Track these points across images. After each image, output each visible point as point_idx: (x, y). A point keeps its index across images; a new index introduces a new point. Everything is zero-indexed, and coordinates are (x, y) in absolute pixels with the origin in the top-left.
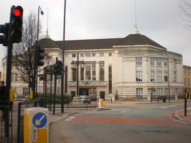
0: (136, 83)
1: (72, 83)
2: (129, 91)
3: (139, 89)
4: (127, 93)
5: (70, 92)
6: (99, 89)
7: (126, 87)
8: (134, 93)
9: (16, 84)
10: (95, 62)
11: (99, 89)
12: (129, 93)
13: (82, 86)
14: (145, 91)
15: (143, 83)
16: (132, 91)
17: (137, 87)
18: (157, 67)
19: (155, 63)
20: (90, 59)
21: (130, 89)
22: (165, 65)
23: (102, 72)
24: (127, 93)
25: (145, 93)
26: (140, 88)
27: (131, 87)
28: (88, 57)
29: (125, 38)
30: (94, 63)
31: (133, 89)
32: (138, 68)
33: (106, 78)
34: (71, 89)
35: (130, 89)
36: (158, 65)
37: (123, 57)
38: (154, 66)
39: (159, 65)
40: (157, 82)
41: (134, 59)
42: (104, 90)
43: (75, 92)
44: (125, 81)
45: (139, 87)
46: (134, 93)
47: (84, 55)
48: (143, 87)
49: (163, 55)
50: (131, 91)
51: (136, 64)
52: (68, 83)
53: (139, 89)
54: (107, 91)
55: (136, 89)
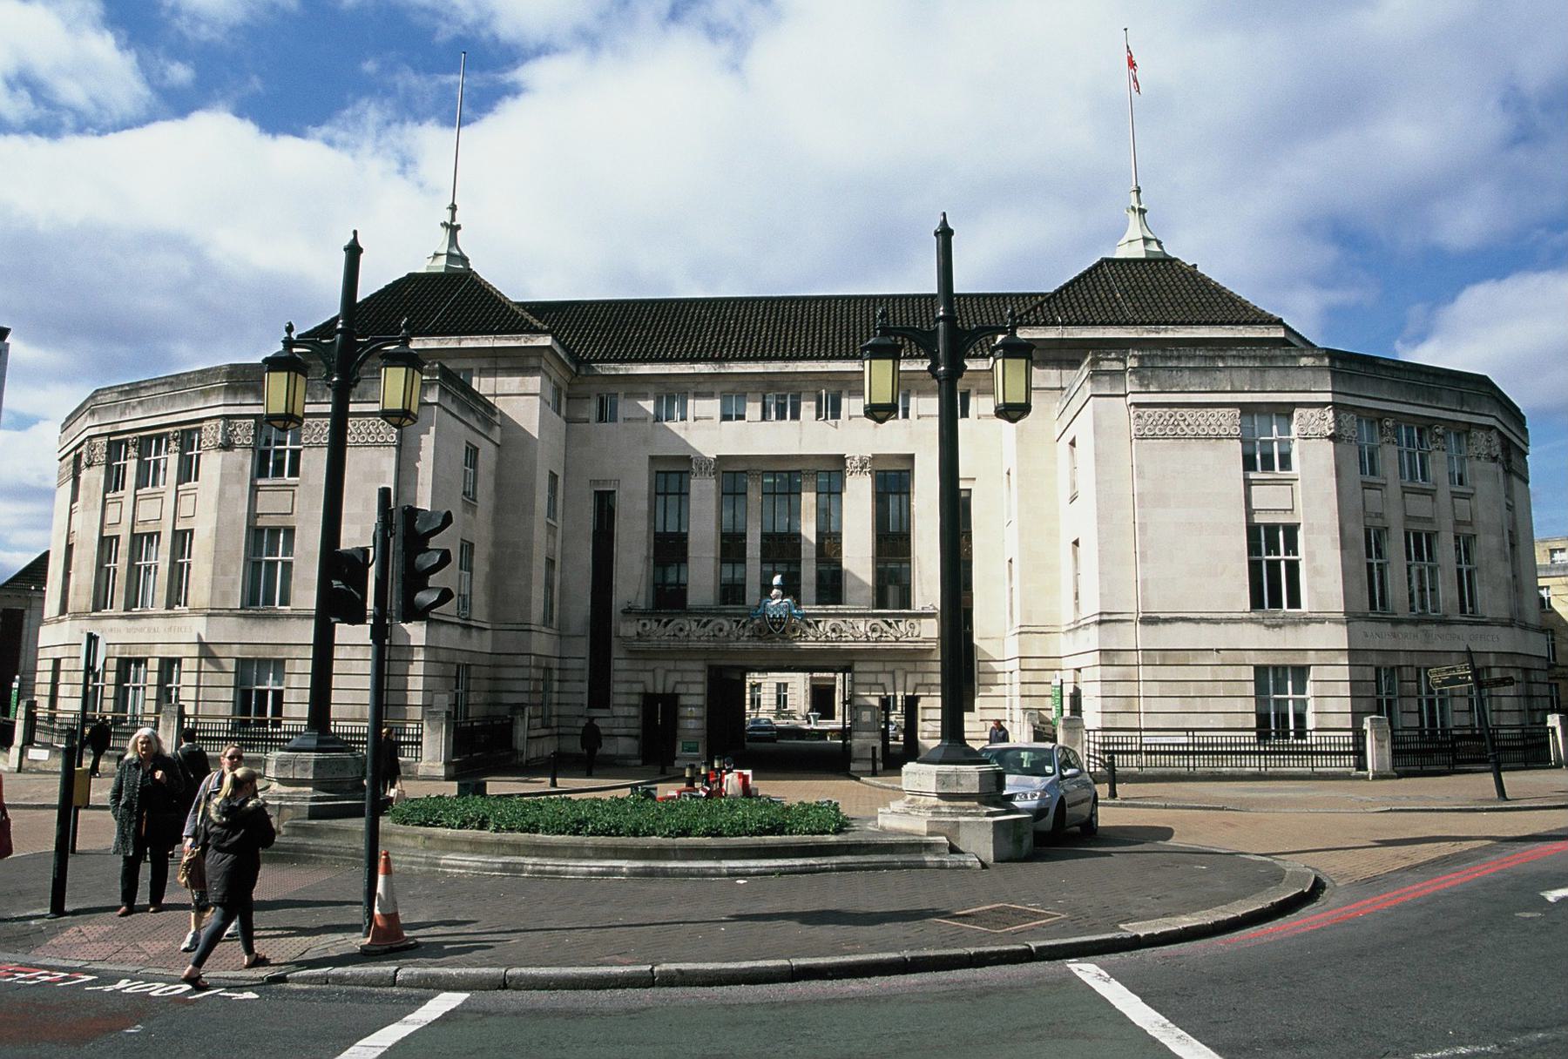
0: (1251, 621)
1: (652, 626)
2: (1192, 689)
3: (1278, 677)
4: (1174, 705)
5: (635, 700)
6: (870, 678)
7: (1167, 656)
8: (1239, 705)
9: (177, 622)
10: (841, 459)
11: (870, 678)
12: (1198, 705)
13: (738, 652)
14: (1330, 689)
15: (1308, 621)
16: (1221, 689)
17: (1263, 660)
18: (1405, 491)
19: (1389, 457)
20: (802, 436)
21: (1207, 673)
22: (1452, 482)
23: (892, 543)
24: (1174, 705)
25: (1327, 703)
26: (1285, 667)
27: (1214, 658)
28: (781, 416)
29: (1053, 295)
30: (830, 473)
31: (1228, 673)
32: (1261, 496)
33: (927, 587)
34: (642, 676)
35: (1207, 673)
36: (1406, 482)
37: (1131, 398)
38: (1381, 487)
39: (1413, 477)
40: (1413, 615)
41: (1229, 420)
42: (673, 678)
43: (982, 775)
44: (1156, 607)
45: (1279, 660)
46: (1239, 705)
47: (753, 409)
48: (1311, 658)
49: (1439, 400)
50: (1208, 689)
51: (1249, 464)
52: (626, 629)
53: (1280, 670)
54: (624, 676)
55: (1249, 674)
